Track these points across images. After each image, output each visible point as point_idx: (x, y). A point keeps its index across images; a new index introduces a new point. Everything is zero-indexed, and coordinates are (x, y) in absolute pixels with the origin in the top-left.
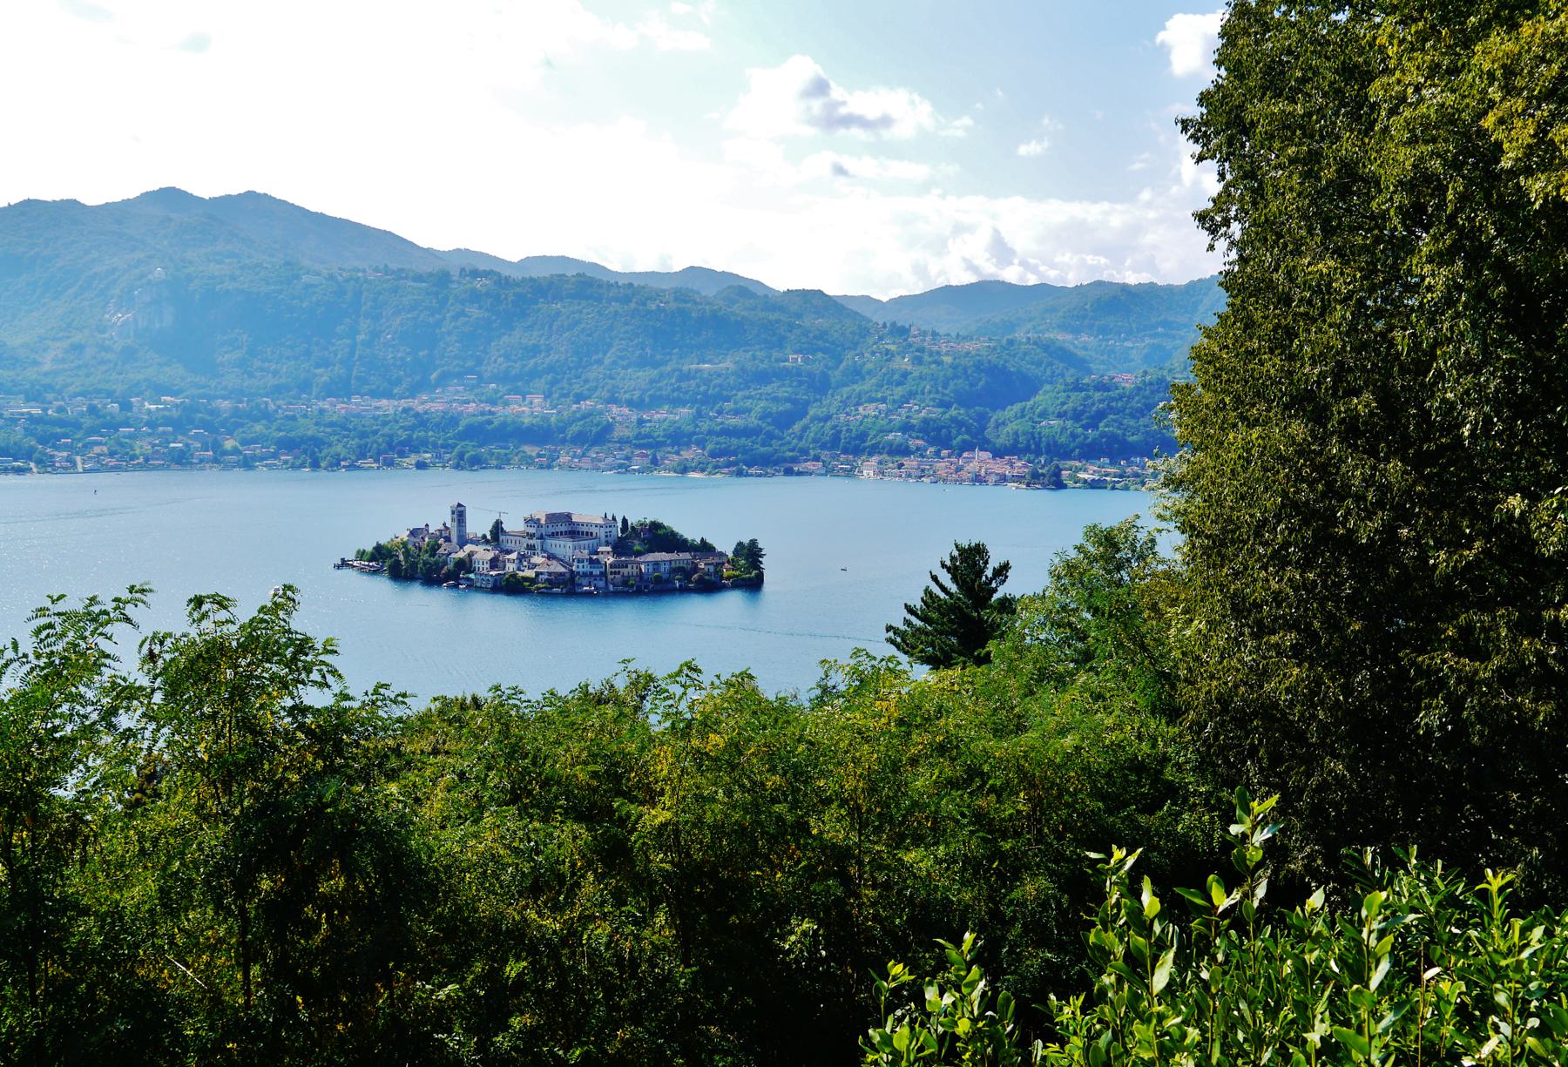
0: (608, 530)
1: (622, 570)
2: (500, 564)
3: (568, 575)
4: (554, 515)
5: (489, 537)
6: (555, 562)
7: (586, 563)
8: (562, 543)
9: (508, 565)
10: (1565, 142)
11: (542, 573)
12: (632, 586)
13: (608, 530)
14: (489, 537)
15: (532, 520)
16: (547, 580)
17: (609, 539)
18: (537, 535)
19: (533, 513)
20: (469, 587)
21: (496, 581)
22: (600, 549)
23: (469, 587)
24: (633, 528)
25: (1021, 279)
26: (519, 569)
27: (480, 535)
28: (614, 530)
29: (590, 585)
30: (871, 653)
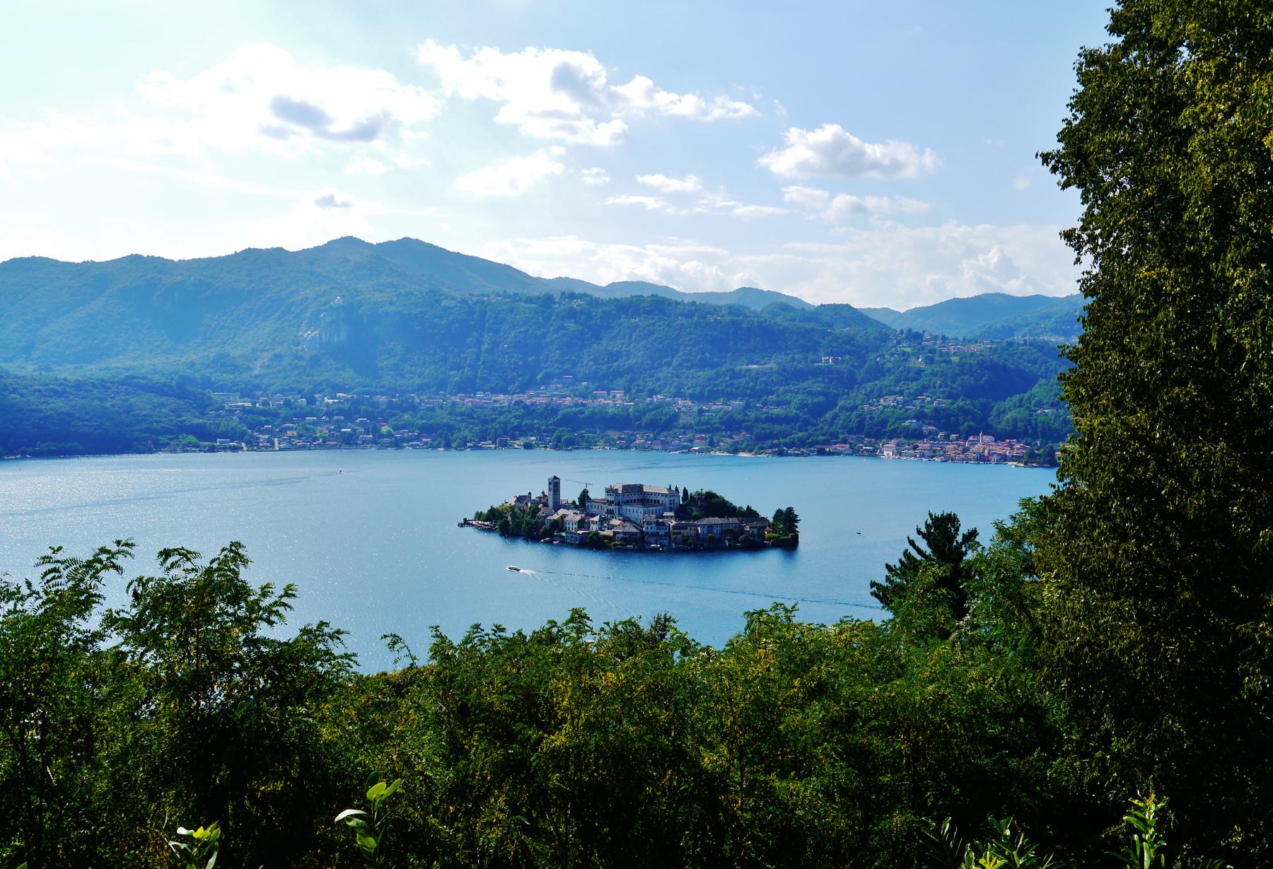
0: (672, 498)
1: (683, 531)
2: (585, 525)
3: (639, 535)
4: (628, 486)
5: (578, 503)
6: (628, 524)
7: (653, 525)
8: (635, 509)
9: (592, 526)
11: (618, 533)
12: (691, 544)
13: (672, 498)
14: (578, 503)
16: (622, 538)
17: (672, 506)
21: (582, 538)
26: (600, 529)
28: (676, 499)
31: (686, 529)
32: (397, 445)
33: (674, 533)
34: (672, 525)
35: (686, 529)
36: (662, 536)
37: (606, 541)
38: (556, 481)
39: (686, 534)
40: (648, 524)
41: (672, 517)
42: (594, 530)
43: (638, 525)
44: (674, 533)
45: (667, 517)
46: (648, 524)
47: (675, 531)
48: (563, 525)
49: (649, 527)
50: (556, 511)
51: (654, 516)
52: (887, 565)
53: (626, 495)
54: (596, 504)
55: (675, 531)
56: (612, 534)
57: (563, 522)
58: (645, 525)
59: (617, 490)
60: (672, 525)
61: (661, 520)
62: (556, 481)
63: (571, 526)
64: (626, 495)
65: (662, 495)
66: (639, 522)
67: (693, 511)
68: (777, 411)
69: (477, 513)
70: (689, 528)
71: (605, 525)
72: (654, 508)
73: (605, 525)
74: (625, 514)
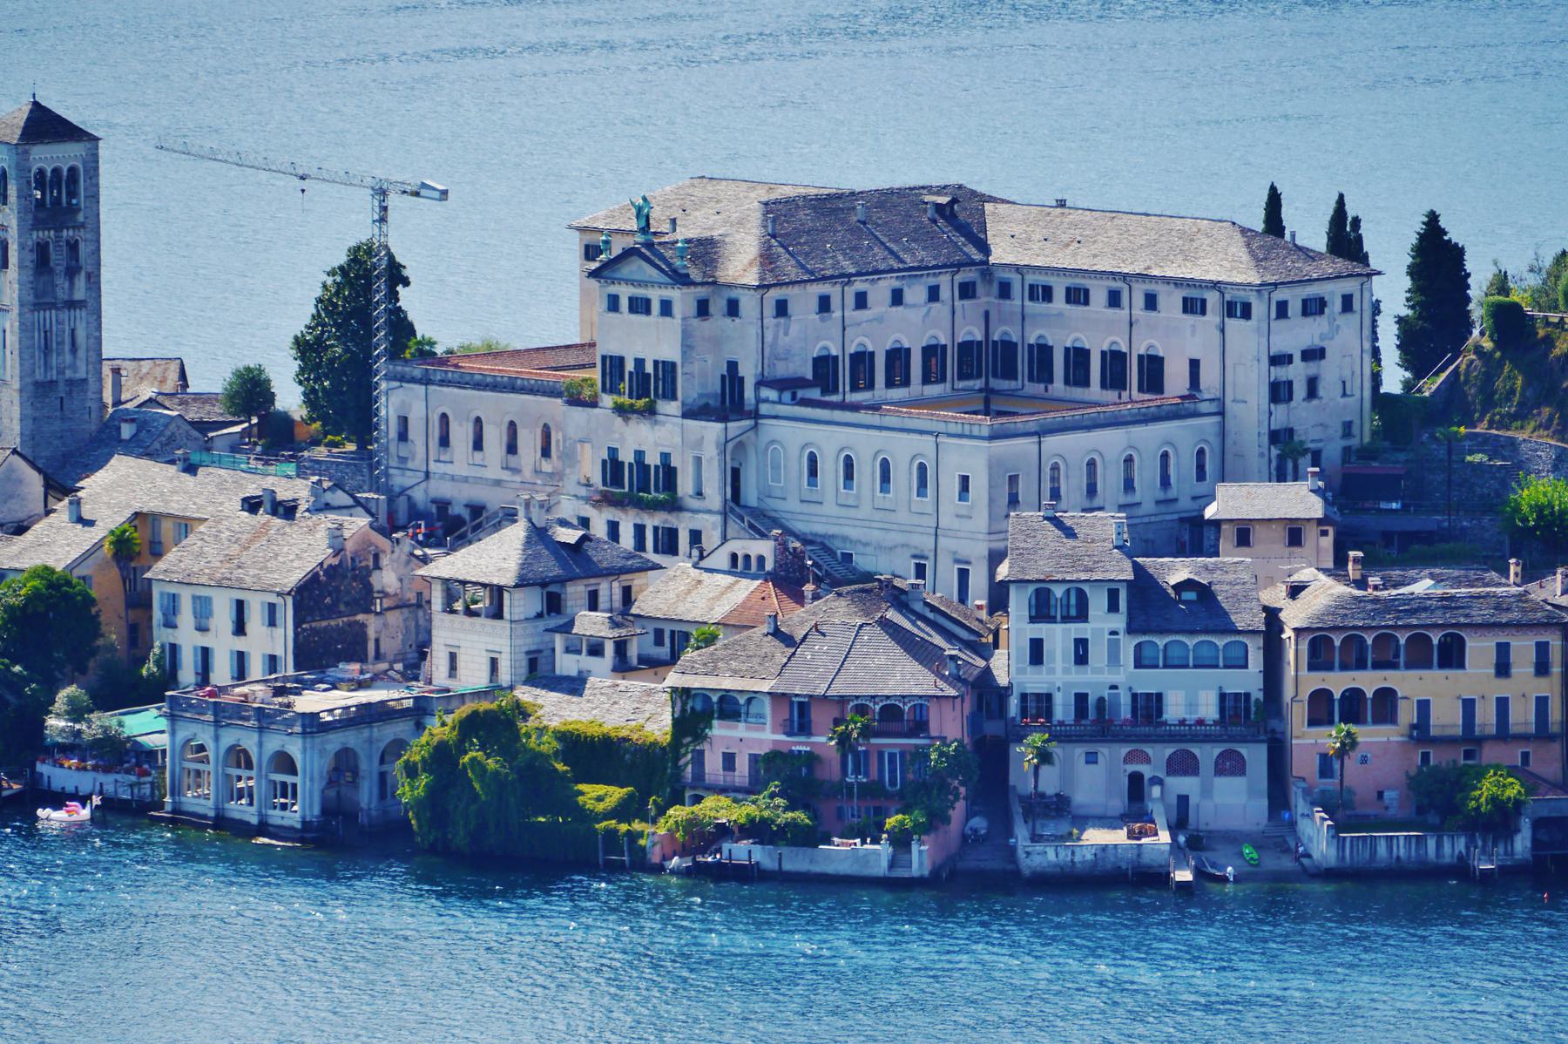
0: (1296, 334)
1: (1409, 684)
2: (383, 629)
3: (950, 727)
4: (831, 206)
5: (289, 398)
6: (837, 611)
7: (1103, 623)
8: (904, 450)
9: (447, 632)
10: (2, 976)
11: (729, 707)
12: (1501, 820)
13: (1296, 334)
14: (289, 398)
15: (648, 248)
16: (770, 765)
17: (1301, 415)
18: (699, 380)
19: (662, 191)
20: (113, 812)
21: (344, 767)
22: (1226, 503)
23: (113, 812)
24: (1508, 319)
25: (1319, 366)
26: (538, 671)
27: (211, 378)
28: (1342, 336)
29: (1135, 812)
30: (864, 540)
31: (1452, 655)
32: (852, 194)
33: (1321, 708)
34: (1294, 615)
35: (1452, 655)
36: (1194, 732)
37: (599, 796)
38: (52, 156)
39: (1446, 718)
40: (1042, 610)
41: (1294, 533)
42: (473, 676)
43: (937, 619)
44: (1321, 708)
45: (1244, 534)
46: (1042, 610)
47: (1338, 682)
48: (138, 635)
49: (1058, 636)
50: (60, 484)
51: (1105, 526)
52: (1433, 218)
53: (803, 300)
54: (496, 408)
55: (1338, 682)
56: (658, 725)
57: (138, 599)
58: (1017, 624)
59: (706, 250)
60: (1294, 615)
61: (1176, 571)
62: (52, 156)
63: (223, 644)
64: (803, 300)
65: (744, 287)
66: (941, 590)
67: (1516, 467)
68: (1462, 620)
69: (1161, 360)
70: (1480, 649)
71: (591, 623)
72: (1110, 443)
73: (591, 623)
74: (791, 506)
